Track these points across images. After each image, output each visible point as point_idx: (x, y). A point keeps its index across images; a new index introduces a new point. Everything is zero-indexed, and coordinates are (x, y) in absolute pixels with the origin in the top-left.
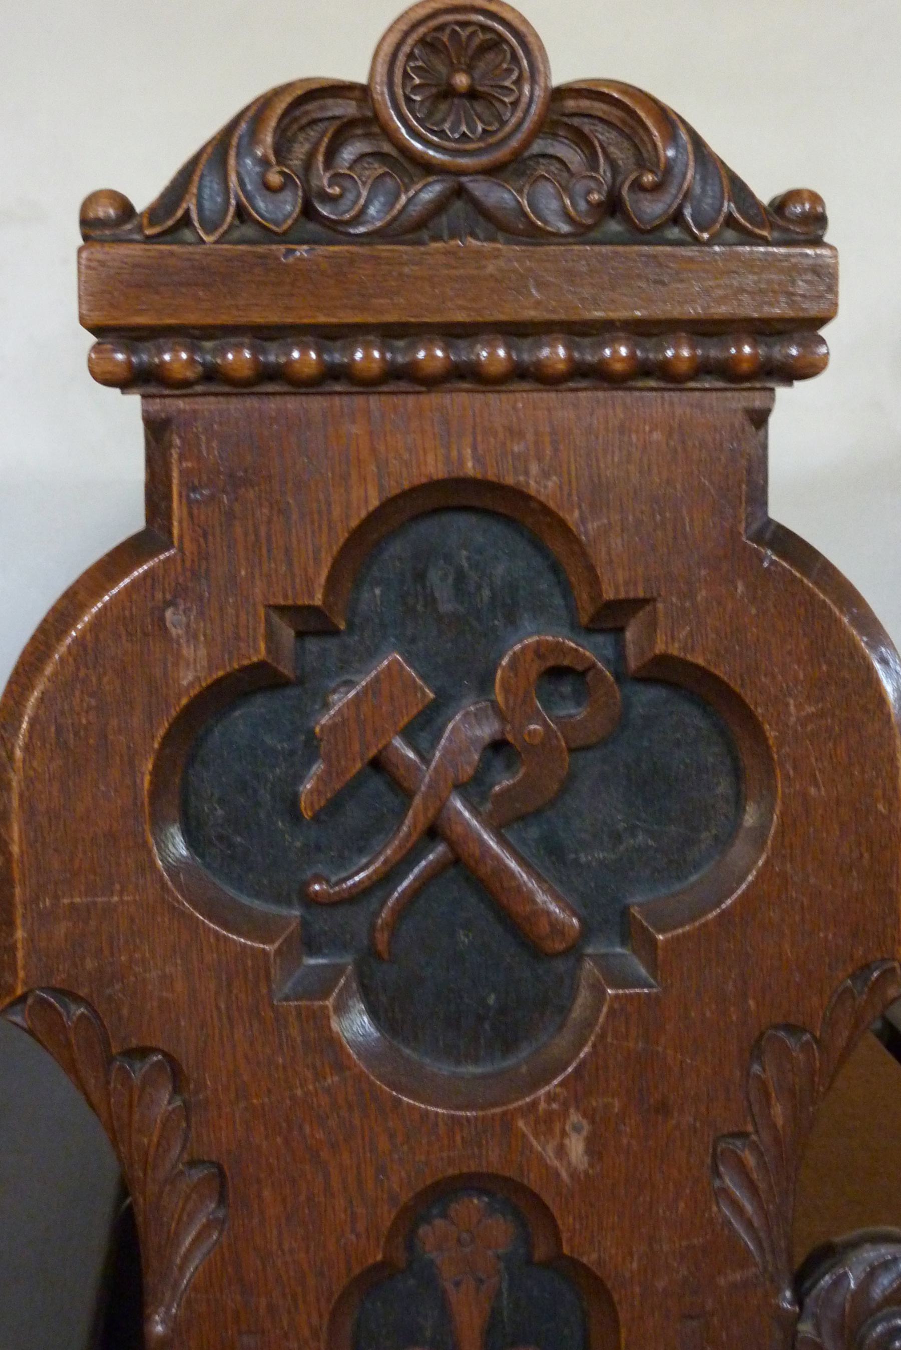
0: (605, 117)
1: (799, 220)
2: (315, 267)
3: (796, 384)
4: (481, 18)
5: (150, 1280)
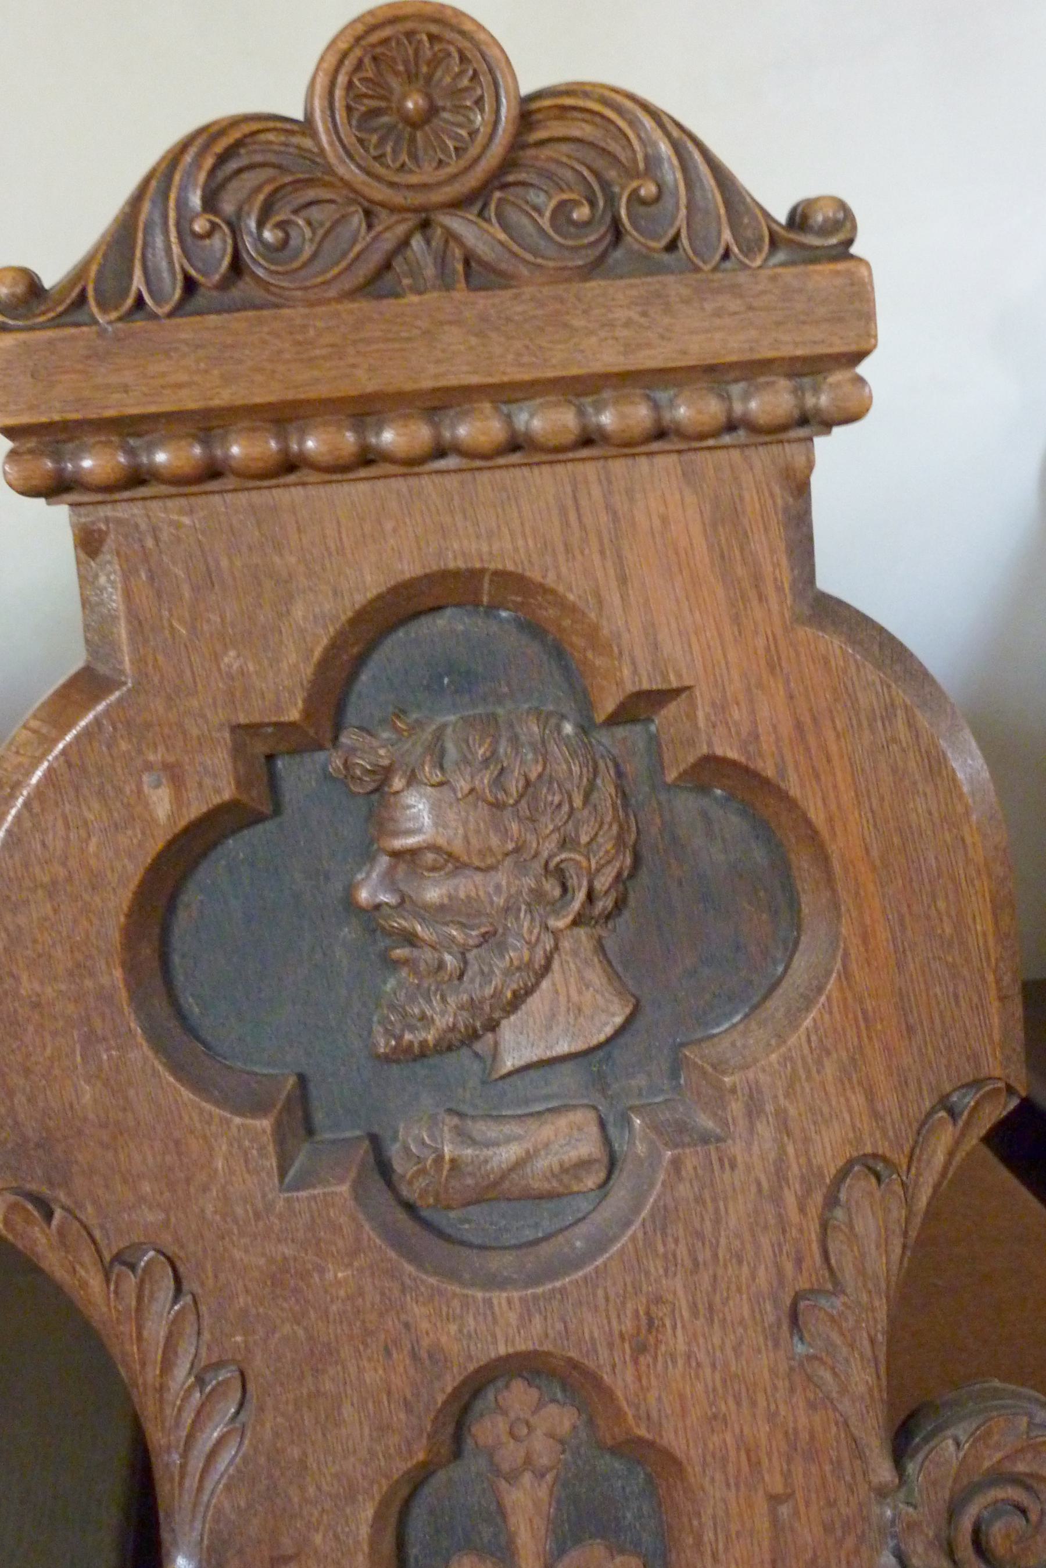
1: (819, 235)
3: (836, 430)
5: (165, 1536)
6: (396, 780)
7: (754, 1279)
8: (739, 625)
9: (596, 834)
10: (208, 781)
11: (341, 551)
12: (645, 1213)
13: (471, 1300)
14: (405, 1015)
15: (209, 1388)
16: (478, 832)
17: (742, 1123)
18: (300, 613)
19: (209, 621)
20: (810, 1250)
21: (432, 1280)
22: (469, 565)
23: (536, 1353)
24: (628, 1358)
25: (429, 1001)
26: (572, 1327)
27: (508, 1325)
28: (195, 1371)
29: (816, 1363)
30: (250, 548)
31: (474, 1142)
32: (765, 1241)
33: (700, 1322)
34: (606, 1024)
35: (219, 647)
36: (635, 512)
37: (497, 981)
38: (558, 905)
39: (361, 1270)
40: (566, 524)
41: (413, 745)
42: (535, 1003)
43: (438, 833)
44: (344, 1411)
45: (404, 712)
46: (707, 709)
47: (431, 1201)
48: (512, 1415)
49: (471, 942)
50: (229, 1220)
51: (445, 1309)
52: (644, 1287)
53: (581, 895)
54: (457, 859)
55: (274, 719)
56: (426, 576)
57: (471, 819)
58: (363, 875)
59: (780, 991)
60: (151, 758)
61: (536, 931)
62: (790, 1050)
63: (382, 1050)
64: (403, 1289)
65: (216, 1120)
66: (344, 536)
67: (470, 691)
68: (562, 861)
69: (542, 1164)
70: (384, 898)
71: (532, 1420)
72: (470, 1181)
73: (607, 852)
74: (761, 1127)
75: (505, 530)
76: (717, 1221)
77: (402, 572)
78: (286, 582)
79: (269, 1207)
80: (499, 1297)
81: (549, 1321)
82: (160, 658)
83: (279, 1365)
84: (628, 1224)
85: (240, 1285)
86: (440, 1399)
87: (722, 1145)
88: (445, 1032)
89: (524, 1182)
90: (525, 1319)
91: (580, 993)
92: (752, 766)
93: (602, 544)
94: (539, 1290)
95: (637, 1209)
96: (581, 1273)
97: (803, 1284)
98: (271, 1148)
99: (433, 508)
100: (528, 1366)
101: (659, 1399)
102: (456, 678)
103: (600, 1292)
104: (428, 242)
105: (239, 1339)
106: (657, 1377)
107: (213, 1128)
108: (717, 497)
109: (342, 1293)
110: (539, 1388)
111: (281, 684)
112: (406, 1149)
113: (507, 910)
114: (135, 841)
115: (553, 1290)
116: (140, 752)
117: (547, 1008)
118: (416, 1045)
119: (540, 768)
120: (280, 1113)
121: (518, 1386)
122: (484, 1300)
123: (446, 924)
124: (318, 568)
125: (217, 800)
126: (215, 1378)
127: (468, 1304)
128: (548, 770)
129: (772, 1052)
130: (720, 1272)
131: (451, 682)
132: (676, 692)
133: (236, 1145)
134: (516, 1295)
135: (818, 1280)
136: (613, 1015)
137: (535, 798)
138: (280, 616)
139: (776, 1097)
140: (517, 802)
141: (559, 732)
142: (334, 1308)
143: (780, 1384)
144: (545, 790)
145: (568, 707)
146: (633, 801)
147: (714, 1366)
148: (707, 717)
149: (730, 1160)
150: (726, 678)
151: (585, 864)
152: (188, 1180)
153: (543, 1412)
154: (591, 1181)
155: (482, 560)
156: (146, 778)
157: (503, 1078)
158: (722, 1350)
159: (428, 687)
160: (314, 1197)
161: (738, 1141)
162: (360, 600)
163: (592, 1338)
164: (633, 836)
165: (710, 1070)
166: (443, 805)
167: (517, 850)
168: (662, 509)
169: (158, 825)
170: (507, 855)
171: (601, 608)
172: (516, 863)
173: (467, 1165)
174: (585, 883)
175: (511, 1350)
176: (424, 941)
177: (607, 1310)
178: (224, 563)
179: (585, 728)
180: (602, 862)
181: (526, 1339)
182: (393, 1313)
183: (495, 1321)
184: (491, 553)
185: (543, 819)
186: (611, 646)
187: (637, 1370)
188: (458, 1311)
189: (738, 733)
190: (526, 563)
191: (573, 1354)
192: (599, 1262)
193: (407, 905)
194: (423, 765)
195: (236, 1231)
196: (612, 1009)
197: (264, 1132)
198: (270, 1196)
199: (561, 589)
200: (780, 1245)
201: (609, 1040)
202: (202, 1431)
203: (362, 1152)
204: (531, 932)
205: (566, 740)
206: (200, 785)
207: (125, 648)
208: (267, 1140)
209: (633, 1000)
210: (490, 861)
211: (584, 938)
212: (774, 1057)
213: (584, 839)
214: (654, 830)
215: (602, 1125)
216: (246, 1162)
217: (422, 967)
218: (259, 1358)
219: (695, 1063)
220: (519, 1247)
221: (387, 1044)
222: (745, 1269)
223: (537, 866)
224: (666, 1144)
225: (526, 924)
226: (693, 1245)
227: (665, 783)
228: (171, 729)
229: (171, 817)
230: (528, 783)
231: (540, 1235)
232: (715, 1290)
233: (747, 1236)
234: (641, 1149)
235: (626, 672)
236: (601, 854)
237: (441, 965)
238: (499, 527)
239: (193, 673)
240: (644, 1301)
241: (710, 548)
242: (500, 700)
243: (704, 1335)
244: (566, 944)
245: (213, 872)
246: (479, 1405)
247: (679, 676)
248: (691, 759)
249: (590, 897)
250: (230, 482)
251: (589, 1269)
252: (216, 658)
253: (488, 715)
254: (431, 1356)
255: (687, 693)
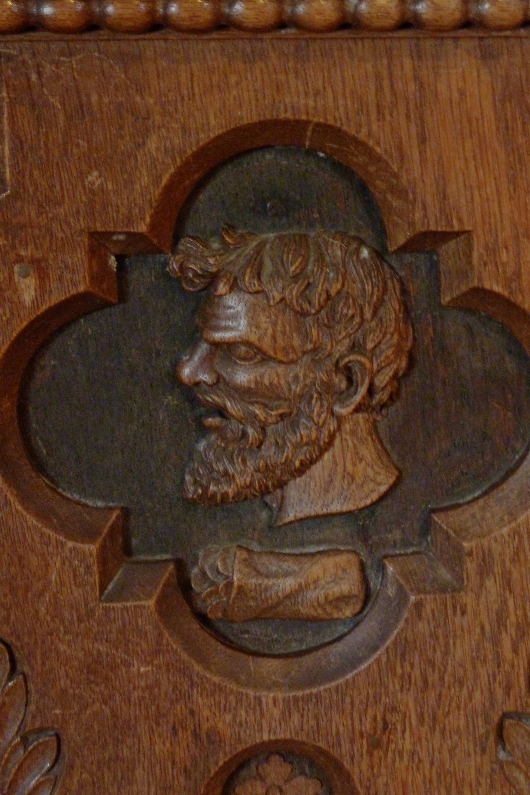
6: (221, 285)
7: (471, 700)
8: (514, 184)
9: (380, 343)
10: (67, 276)
11: (192, 97)
12: (388, 642)
13: (244, 697)
14: (211, 470)
15: (31, 748)
16: (284, 333)
17: (474, 580)
18: (154, 145)
19: (78, 145)
20: (518, 680)
21: (216, 679)
22: (297, 117)
23: (292, 741)
24: (364, 751)
25: (232, 462)
26: (322, 724)
27: (272, 717)
28: (21, 733)
29: (513, 767)
30: (117, 89)
31: (259, 573)
32: (483, 672)
33: (424, 729)
34: (373, 491)
35: (84, 167)
36: (439, 85)
37: (288, 452)
38: (345, 395)
39: (159, 667)
40: (379, 88)
41: (239, 256)
42: (317, 469)
43: (251, 331)
44: (137, 773)
45: (233, 228)
46: (482, 251)
47: (220, 615)
48: (269, 781)
49: (270, 420)
50: (57, 620)
51: (223, 702)
52: (383, 698)
53: (362, 390)
54: (264, 353)
55: (126, 230)
56: (260, 122)
57: (280, 322)
58: (188, 357)
59: (516, 476)
60: (23, 253)
61: (323, 416)
62: (519, 526)
63: (190, 496)
64: (192, 685)
65: (53, 542)
66: (195, 84)
67: (287, 216)
68: (350, 362)
69: (311, 595)
70: (205, 377)
71: (284, 788)
72: (252, 603)
73: (387, 357)
74: (489, 583)
75: (329, 91)
76: (446, 653)
77: (241, 118)
78: (144, 119)
79: (90, 614)
80: (267, 697)
81: (305, 718)
82: (36, 173)
83: (88, 734)
84: (375, 648)
85: (62, 672)
86: (213, 770)
87: (457, 596)
88: (242, 487)
89: (294, 608)
90: (286, 716)
91: (354, 465)
92: (512, 299)
93: (408, 108)
94: (300, 694)
95: (383, 638)
96: (334, 684)
97: (509, 707)
98: (95, 568)
99: (271, 69)
100: (286, 751)
101: (386, 785)
102: (278, 206)
103: (348, 700)
104: (24, 753)
105: (57, 711)
106: (386, 767)
107: (50, 549)
108: (507, 77)
109: (142, 684)
110: (291, 763)
111: (134, 200)
112: (204, 573)
113: (301, 396)
114: (4, 318)
115: (311, 694)
116: (14, 247)
117: (326, 474)
118: (219, 496)
119: (339, 286)
120: (105, 540)
121: (275, 760)
122: (255, 697)
123: (252, 403)
124: (172, 109)
125: (73, 291)
126: (38, 739)
127: (241, 701)
128: (346, 287)
129: (504, 526)
130: (444, 692)
131: (273, 207)
132: (458, 234)
133: (67, 563)
134: (280, 695)
135: (522, 705)
136: (379, 484)
137: (333, 310)
138: (138, 146)
139: (503, 562)
140: (318, 312)
141: (358, 257)
142: (135, 694)
143: (483, 781)
144: (342, 304)
145: (367, 234)
146: (413, 315)
147: (432, 763)
148: (481, 256)
149: (461, 608)
150: (499, 227)
151: (368, 365)
152: (27, 588)
153: (293, 782)
154: (348, 612)
155: (308, 114)
156: (16, 268)
157: (285, 525)
158: (440, 751)
159: (253, 209)
160: (126, 609)
161: (469, 593)
162: (204, 138)
163: (338, 733)
164: (409, 344)
165: (452, 534)
166: (258, 309)
167: (315, 350)
168: (461, 84)
169: (25, 308)
170: (304, 353)
171: (402, 160)
172: (313, 360)
173: (250, 591)
174: (367, 381)
175: (273, 738)
176: (233, 416)
177: (352, 714)
178: (94, 98)
179: (380, 254)
180: (383, 364)
181: (285, 731)
182: (182, 701)
183: (262, 715)
184: (315, 108)
185: (337, 327)
186: (407, 192)
187: (371, 761)
188: (234, 704)
189: (505, 272)
190: (344, 120)
191: (322, 744)
192: (349, 676)
193: (221, 385)
194: (244, 275)
195: (62, 629)
196: (379, 480)
197: (91, 555)
198: (92, 605)
199: (371, 143)
200: (494, 675)
201: (374, 504)
202: (23, 779)
203: (167, 574)
204: (319, 416)
205: (363, 263)
206: (61, 278)
207: (7, 161)
208: (93, 560)
209: (396, 473)
210: (292, 356)
211: (361, 421)
212: (505, 530)
213: (370, 345)
214: (427, 340)
215: (362, 567)
216: (75, 576)
217: (229, 435)
218: (72, 727)
219: (441, 527)
220: (286, 656)
221: (196, 491)
222: (465, 691)
223: (329, 364)
224: (412, 590)
225: (316, 410)
226: (425, 670)
227: (440, 303)
228: (40, 230)
229: (36, 302)
230: (329, 297)
231: (304, 648)
232: (439, 706)
233: (469, 667)
234: (391, 591)
235: (418, 215)
236: (382, 358)
237: (244, 435)
238: (324, 88)
239: (62, 187)
240: (382, 709)
241: (497, 119)
242: (311, 225)
243: (427, 740)
244: (347, 427)
245: (68, 342)
246: (244, 773)
247: (460, 220)
248: (464, 288)
249: (371, 391)
250: (104, 33)
251: (341, 681)
252: (82, 176)
253: (301, 236)
254: (208, 736)
255: (466, 235)
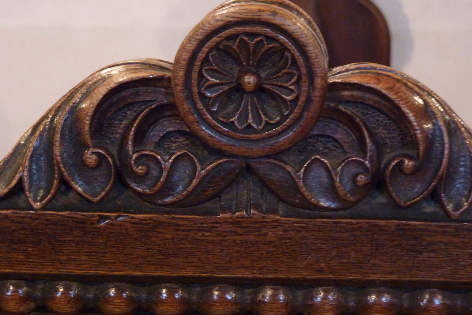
0: (376, 105)
2: (124, 231)
4: (268, 30)
